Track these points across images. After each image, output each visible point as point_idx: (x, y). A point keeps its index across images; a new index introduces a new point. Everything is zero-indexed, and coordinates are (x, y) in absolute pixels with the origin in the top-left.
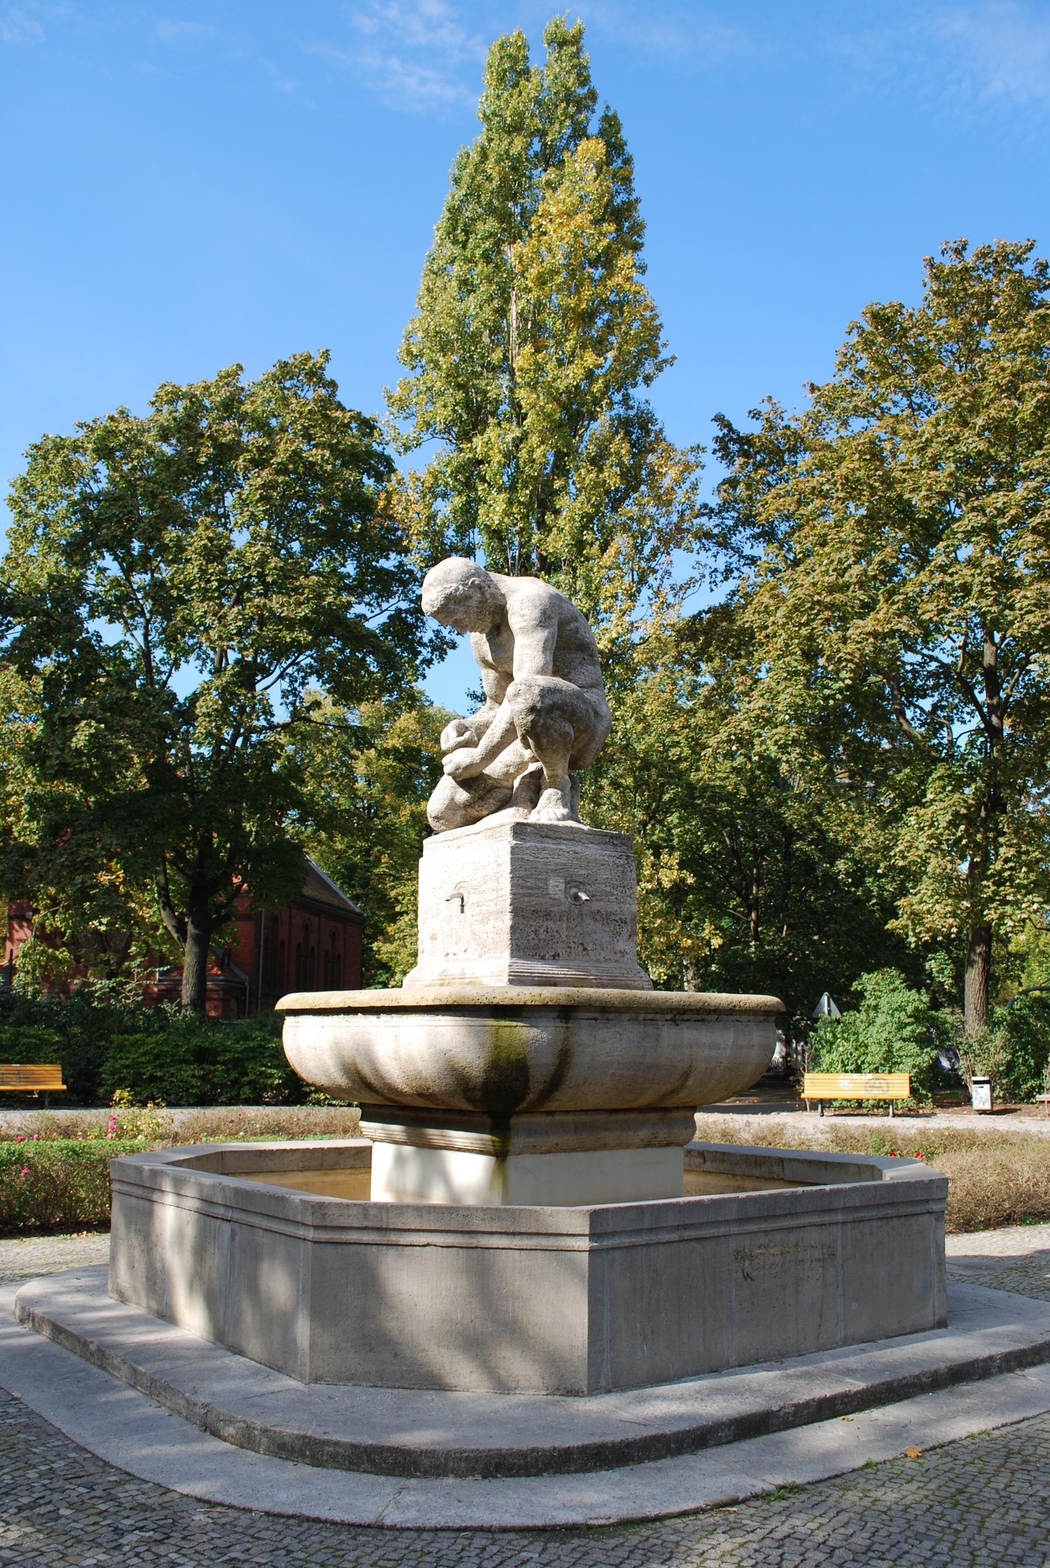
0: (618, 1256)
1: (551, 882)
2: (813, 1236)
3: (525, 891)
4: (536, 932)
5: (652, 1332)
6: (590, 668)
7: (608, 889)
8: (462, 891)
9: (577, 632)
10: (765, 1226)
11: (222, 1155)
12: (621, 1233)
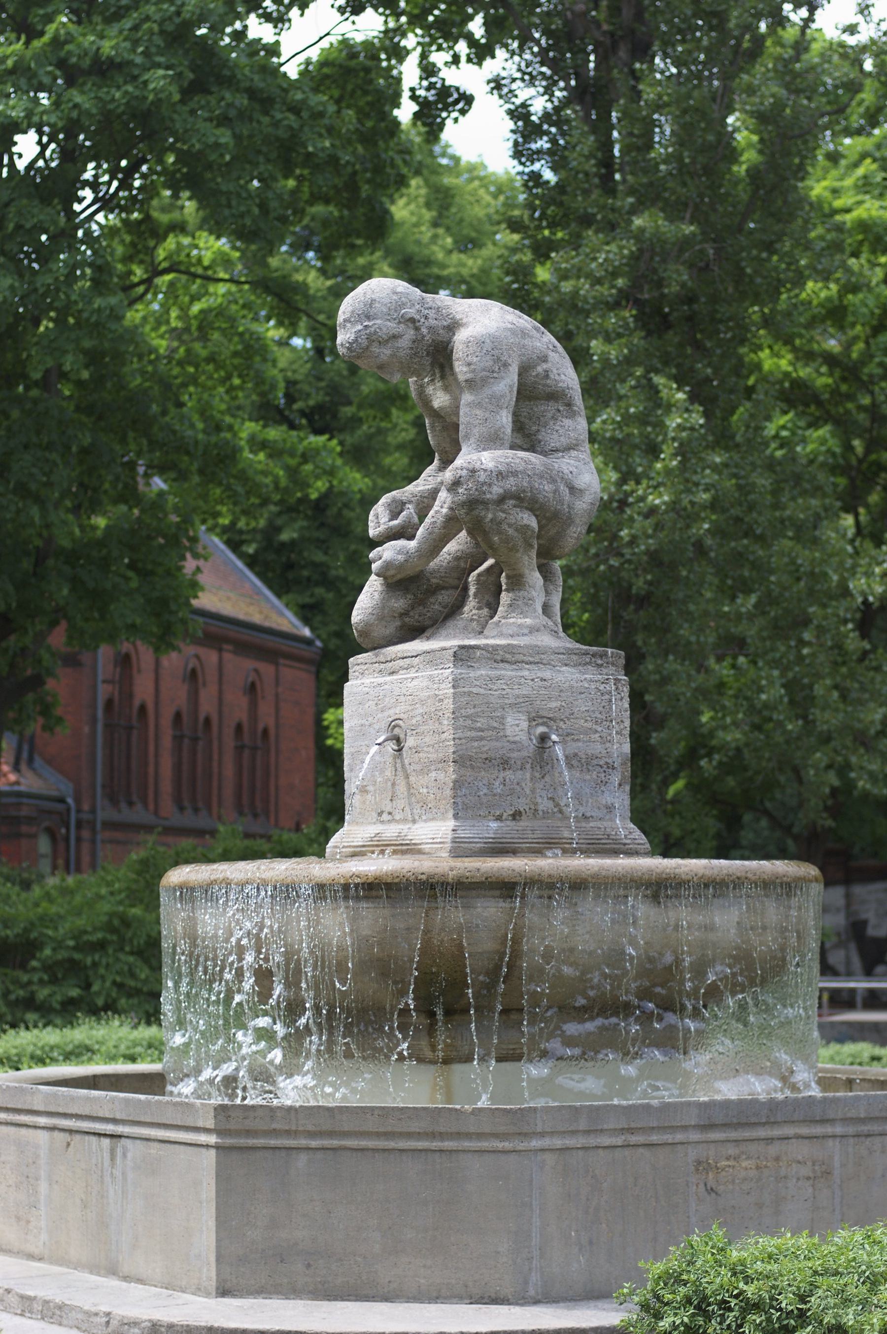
0: (550, 1158)
1: (510, 720)
2: (801, 1150)
3: (473, 734)
4: (489, 785)
5: (591, 1243)
6: (567, 422)
7: (589, 725)
8: (397, 731)
9: (547, 376)
10: (733, 1135)
11: (95, 1077)
12: (552, 1134)
